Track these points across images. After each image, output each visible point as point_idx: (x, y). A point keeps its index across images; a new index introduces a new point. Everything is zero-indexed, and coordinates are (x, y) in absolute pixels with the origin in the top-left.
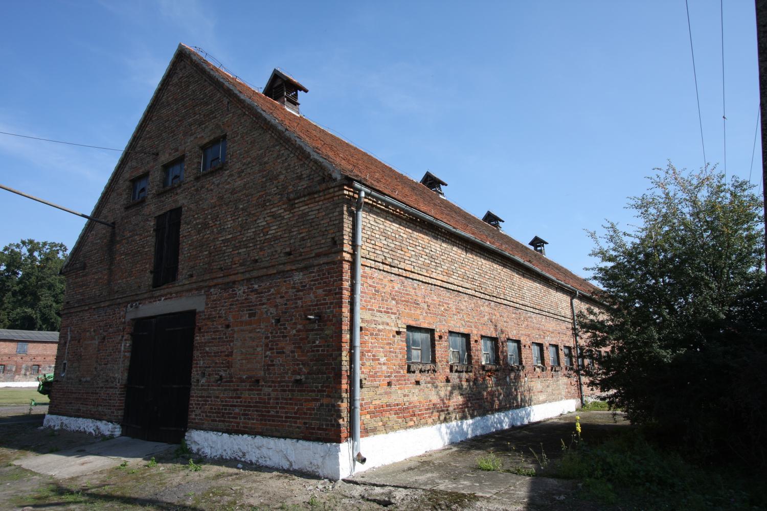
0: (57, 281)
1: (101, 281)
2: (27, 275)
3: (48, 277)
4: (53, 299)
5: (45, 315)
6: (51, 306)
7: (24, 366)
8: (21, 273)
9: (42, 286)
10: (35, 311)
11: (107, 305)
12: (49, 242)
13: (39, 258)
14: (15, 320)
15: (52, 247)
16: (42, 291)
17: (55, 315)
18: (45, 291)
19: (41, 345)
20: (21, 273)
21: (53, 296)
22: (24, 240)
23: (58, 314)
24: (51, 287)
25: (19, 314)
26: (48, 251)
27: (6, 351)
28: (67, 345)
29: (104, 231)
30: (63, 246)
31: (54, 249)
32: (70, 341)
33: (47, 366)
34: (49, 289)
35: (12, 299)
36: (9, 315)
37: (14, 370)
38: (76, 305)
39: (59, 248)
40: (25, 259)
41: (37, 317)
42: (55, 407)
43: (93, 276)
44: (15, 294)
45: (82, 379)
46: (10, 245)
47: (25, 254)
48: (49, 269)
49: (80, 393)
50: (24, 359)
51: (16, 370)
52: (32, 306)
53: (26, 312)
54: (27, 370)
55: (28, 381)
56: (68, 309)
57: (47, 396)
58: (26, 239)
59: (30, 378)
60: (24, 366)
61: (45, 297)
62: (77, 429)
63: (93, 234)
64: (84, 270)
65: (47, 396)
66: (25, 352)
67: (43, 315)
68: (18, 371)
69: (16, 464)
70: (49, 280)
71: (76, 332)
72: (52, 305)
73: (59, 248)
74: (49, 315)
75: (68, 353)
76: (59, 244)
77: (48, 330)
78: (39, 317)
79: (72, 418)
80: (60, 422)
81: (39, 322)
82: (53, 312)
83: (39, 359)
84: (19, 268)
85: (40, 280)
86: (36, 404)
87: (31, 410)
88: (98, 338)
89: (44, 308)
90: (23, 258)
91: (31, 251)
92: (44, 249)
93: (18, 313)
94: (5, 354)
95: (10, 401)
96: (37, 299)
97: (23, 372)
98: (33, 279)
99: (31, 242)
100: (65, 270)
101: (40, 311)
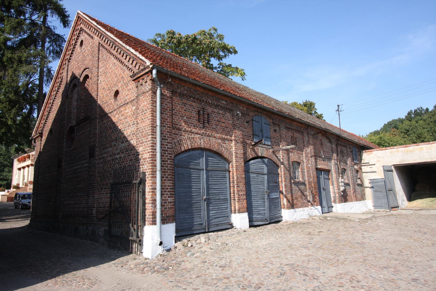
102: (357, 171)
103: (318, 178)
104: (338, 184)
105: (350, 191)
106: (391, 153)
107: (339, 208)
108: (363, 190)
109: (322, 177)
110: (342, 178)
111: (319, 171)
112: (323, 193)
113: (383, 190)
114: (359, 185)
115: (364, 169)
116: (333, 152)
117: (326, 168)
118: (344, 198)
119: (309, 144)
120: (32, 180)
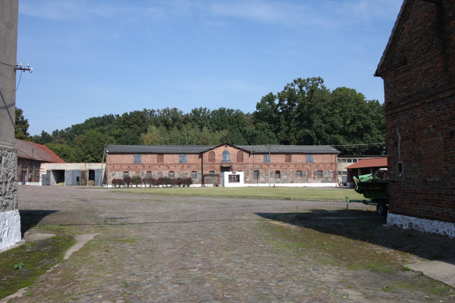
0: (322, 106)
1: (432, 70)
2: (301, 106)
3: (315, 104)
4: (321, 121)
5: (318, 133)
6: (321, 126)
7: (312, 171)
8: (297, 104)
9: (312, 112)
10: (312, 131)
11: (448, 95)
12: (310, 78)
13: (306, 91)
14: (301, 139)
15: (313, 81)
16: (313, 116)
17: (325, 133)
18: (315, 115)
19: (321, 156)
20: (297, 104)
21: (321, 119)
22: (295, 79)
23: (327, 132)
24: (318, 111)
25: (302, 134)
26: (311, 85)
27: (300, 161)
28: (399, 145)
29: (426, 14)
30: (321, 79)
31: (315, 82)
32: (401, 141)
33: (327, 171)
34: (318, 113)
35: (295, 124)
36: (295, 136)
37: (307, 175)
38: (402, 104)
39: (318, 81)
40: (298, 93)
41: (313, 135)
42: (398, 206)
43: (419, 68)
44: (296, 119)
45: (428, 179)
46: (288, 85)
47: (297, 90)
48: (315, 98)
49: (427, 194)
50: (312, 167)
51: (308, 174)
52: (309, 128)
53: (306, 132)
54: (314, 174)
55: (317, 183)
56: (392, 109)
57: (362, 195)
58: (296, 79)
59: (318, 180)
60: (312, 171)
61: (317, 119)
62: (434, 231)
63: (410, 23)
64: (405, 64)
65: (362, 195)
66: (311, 161)
67: (317, 133)
68: (309, 176)
69: (415, 269)
70: (317, 106)
71: (407, 131)
72: (321, 125)
73: (318, 81)
74: (321, 133)
75: (402, 153)
76: (317, 78)
77: (322, 145)
78: (315, 135)
79: (423, 220)
80: (408, 222)
81: (316, 139)
82: (323, 131)
83: (321, 166)
84: (295, 101)
85: (310, 108)
86: (351, 201)
87: (347, 205)
88: (442, 133)
89: (317, 128)
90: (297, 93)
91: (300, 87)
92: (309, 84)
93: (301, 134)
94: (300, 163)
95: (319, 197)
96: (311, 122)
97: (312, 176)
98: (305, 108)
99: (300, 80)
100: (381, 71)
101: (315, 130)
102: (37, 171)
103: (22, 174)
104: (29, 175)
105: (33, 178)
106: (51, 165)
107: (27, 183)
108: (39, 178)
109: (23, 173)
110: (31, 174)
111: (23, 171)
112: (23, 179)
113: (46, 179)
114: (37, 176)
115: (41, 170)
116: (28, 165)
117: (25, 170)
118: (30, 180)
119: (21, 164)
120: (349, 209)
